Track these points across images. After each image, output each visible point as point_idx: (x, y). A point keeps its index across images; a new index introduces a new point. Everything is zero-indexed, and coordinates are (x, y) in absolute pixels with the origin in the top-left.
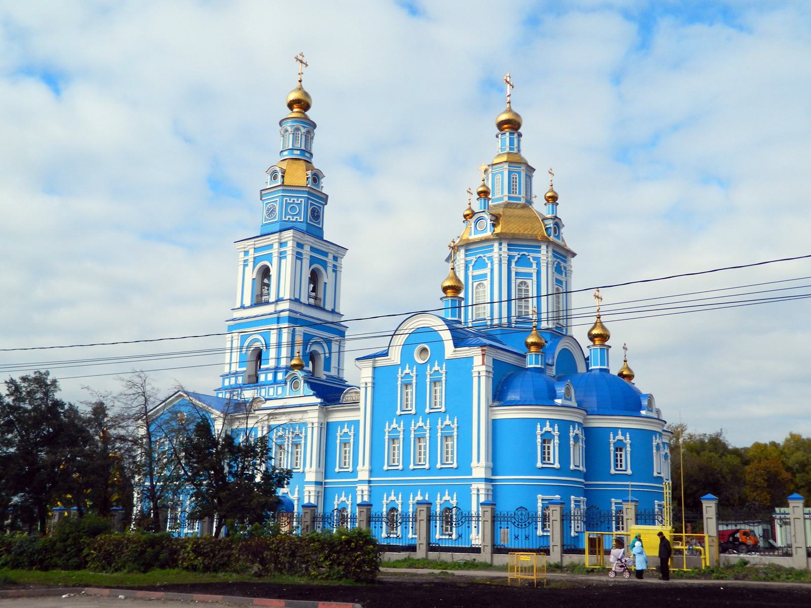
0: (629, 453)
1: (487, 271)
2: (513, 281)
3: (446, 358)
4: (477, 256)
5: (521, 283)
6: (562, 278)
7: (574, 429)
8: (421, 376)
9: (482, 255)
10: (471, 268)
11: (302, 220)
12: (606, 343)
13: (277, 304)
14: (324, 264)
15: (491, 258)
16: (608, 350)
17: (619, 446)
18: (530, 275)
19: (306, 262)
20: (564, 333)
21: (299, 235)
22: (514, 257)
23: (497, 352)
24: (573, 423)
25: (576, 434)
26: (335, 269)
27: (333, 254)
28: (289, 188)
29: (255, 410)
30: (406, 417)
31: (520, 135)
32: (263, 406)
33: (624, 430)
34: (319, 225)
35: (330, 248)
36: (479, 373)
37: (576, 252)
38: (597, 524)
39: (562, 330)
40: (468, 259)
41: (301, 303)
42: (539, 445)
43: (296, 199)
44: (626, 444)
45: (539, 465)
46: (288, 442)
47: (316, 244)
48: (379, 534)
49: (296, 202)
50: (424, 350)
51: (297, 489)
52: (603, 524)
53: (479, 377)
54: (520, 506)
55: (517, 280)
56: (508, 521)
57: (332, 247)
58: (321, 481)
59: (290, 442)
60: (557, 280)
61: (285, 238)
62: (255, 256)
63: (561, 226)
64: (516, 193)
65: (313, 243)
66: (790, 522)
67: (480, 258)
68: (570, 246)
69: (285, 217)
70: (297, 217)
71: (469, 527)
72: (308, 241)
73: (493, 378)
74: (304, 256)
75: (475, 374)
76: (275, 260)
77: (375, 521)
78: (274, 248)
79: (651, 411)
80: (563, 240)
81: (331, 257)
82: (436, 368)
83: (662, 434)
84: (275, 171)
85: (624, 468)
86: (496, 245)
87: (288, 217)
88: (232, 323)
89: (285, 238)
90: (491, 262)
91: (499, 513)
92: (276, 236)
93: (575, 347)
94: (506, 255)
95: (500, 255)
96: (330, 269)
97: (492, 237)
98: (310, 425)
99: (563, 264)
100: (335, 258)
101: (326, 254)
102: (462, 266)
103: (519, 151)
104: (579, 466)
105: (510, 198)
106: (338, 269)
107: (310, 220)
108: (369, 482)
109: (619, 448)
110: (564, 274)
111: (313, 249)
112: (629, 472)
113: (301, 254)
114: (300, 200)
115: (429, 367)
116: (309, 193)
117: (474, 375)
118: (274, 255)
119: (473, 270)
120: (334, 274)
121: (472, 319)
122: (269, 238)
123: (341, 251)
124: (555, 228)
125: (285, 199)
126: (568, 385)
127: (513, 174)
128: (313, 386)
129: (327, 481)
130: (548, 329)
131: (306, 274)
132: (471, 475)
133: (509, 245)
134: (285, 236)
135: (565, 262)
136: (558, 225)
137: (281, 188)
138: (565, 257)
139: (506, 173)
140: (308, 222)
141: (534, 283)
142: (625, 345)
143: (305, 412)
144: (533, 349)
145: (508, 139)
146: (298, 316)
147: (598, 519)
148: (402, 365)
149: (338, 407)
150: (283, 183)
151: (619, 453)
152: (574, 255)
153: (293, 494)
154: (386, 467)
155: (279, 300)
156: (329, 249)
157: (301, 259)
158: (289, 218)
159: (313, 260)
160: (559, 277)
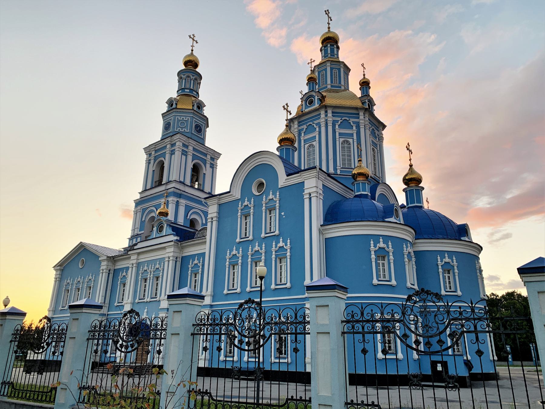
3: (279, 187)
4: (308, 125)
8: (258, 206)
9: (311, 123)
10: (303, 134)
11: (188, 131)
18: (352, 135)
19: (190, 158)
21: (185, 138)
22: (338, 121)
26: (213, 167)
27: (210, 155)
30: (245, 243)
31: (338, 48)
36: (310, 195)
42: (373, 260)
43: (184, 118)
44: (453, 266)
49: (184, 119)
50: (261, 185)
53: (310, 199)
54: (366, 314)
56: (363, 334)
59: (152, 275)
62: (156, 155)
67: (310, 126)
70: (185, 129)
76: (167, 156)
81: (209, 157)
86: (323, 112)
87: (178, 129)
90: (319, 127)
92: (169, 139)
95: (326, 120)
96: (208, 166)
98: (167, 259)
103: (338, 57)
104: (414, 285)
105: (332, 86)
106: (215, 166)
108: (211, 306)
117: (305, 197)
122: (164, 142)
127: (334, 70)
131: (190, 166)
133: (333, 112)
137: (175, 110)
139: (329, 69)
143: (164, 248)
145: (329, 49)
148: (242, 199)
154: (225, 292)
155: (169, 182)
156: (207, 151)
157: (186, 156)
159: (194, 157)
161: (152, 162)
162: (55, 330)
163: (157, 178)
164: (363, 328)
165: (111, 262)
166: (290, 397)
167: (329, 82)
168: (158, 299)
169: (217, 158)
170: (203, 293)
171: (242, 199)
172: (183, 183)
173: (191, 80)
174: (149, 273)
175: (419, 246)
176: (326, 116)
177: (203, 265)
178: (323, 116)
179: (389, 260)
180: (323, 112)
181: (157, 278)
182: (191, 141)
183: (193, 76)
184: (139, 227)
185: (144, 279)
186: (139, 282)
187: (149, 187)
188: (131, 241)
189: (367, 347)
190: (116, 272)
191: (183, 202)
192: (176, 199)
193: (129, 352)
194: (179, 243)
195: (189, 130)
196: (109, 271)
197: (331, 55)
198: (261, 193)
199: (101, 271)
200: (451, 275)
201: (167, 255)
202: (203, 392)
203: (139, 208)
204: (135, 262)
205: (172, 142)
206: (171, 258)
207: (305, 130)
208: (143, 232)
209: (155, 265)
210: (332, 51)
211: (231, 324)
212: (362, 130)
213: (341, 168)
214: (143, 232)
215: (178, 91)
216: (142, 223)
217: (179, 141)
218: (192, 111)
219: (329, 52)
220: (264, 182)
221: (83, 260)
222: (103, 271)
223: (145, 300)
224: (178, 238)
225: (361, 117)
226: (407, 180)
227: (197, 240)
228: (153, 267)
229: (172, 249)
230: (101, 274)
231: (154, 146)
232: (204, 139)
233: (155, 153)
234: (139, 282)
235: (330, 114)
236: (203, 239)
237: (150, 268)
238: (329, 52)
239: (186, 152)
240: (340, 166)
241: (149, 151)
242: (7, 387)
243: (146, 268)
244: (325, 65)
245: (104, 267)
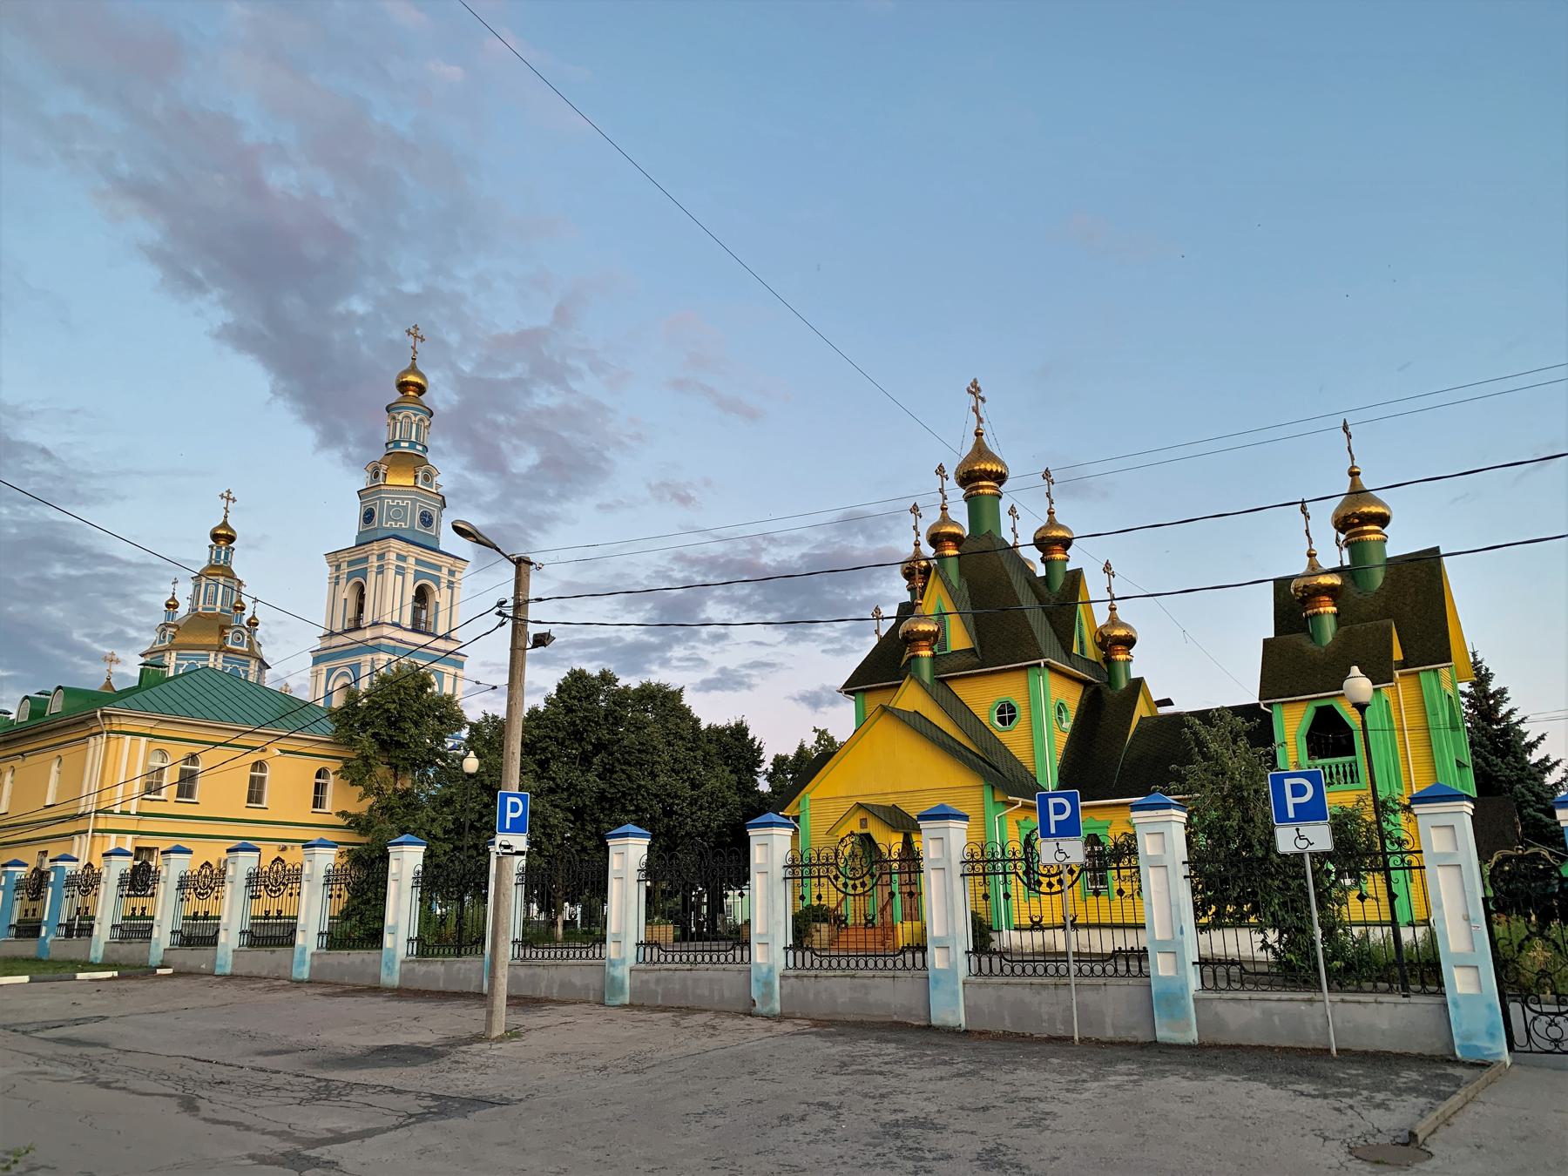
14: (437, 580)
19: (410, 578)
26: (451, 585)
41: (401, 627)
56: (1005, 874)
57: (445, 558)
76: (371, 577)
77: (984, 874)
96: (444, 585)
100: (451, 573)
101: (439, 568)
111: (418, 562)
123: (459, 564)
131: (411, 592)
157: (403, 575)
159: (417, 575)
161: (343, 582)
162: (289, 871)
163: (351, 613)
164: (984, 869)
166: (1117, 949)
183: (415, 415)
193: (859, 895)
202: (913, 947)
203: (323, 667)
211: (832, 864)
218: (415, 489)
239: (403, 568)
242: (648, 950)
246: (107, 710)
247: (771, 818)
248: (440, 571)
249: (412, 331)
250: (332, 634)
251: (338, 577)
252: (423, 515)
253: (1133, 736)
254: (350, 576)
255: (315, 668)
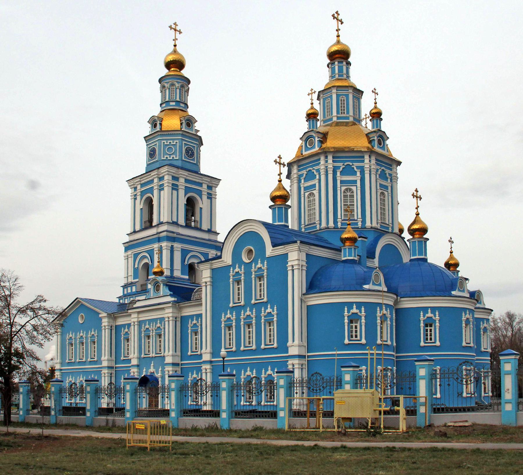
0: (363, 324)
1: (316, 182)
2: (339, 189)
3: (267, 256)
4: (307, 170)
5: (347, 189)
6: (388, 183)
7: (466, 314)
8: (248, 274)
9: (311, 169)
10: (303, 181)
11: (177, 158)
12: (425, 236)
13: (158, 227)
14: (200, 193)
15: (318, 171)
16: (425, 242)
17: (429, 322)
18: (355, 182)
19: (182, 192)
20: (390, 231)
21: (173, 170)
22: (339, 167)
23: (310, 248)
24: (380, 305)
25: (467, 319)
26: (211, 197)
28: (166, 133)
29: (128, 310)
30: (238, 309)
31: (349, 64)
32: (135, 306)
33: (433, 309)
34: (194, 161)
35: (203, 179)
37: (401, 161)
38: (320, 389)
39: (388, 228)
40: (300, 173)
42: (346, 324)
43: (172, 141)
44: (435, 320)
45: (346, 341)
46: (153, 333)
47: (189, 177)
48: (187, 402)
49: (172, 143)
50: (250, 251)
51: (160, 369)
52: (326, 389)
53: (293, 270)
55: (342, 187)
58: (178, 362)
59: (154, 333)
60: (381, 185)
61: (162, 173)
63: (385, 138)
64: (344, 113)
65: (187, 176)
66: (356, 388)
68: (396, 155)
69: (163, 157)
71: (217, 396)
72: (182, 174)
73: (306, 271)
74: (180, 187)
75: (290, 268)
76: (156, 192)
78: (155, 182)
79: (463, 291)
80: (388, 150)
82: (259, 265)
83: (474, 311)
84: (155, 121)
85: (433, 341)
86: (322, 158)
87: (166, 156)
88: (127, 245)
89: (162, 173)
91: (118, 387)
92: (155, 172)
93: (400, 243)
94: (332, 166)
95: (326, 167)
96: (205, 197)
97: (320, 151)
98: (167, 319)
99: (388, 172)
102: (295, 180)
103: (348, 77)
105: (338, 118)
106: (213, 196)
107: (185, 157)
108: (211, 362)
109: (429, 323)
110: (389, 180)
111: (187, 181)
112: (438, 343)
113: (177, 186)
114: (175, 141)
115: (253, 265)
116: (182, 135)
118: (155, 188)
119: (304, 182)
120: (209, 200)
121: (305, 224)
124: (379, 140)
125: (163, 142)
126: (376, 272)
128: (171, 288)
129: (182, 362)
130: (372, 228)
131: (183, 201)
132: (287, 353)
133: (333, 157)
134: (162, 172)
135: (391, 170)
136: (382, 137)
137: (159, 133)
138: (391, 166)
139: (334, 97)
140: (183, 159)
141: (358, 188)
142: (451, 238)
143: (163, 309)
144: (347, 244)
145: (337, 68)
146: (175, 235)
147: (321, 384)
148: (233, 265)
149: (187, 304)
150: (161, 129)
151: (429, 328)
152: (399, 163)
153: (158, 373)
155: (161, 223)
157: (177, 190)
158: (167, 157)
159: (187, 190)
160: (384, 183)
161: (139, 198)
163: (146, 218)
165: (112, 318)
167: (335, 113)
168: (162, 355)
169: (215, 185)
170: (167, 407)
171: (233, 265)
172: (175, 224)
173: (176, 89)
174: (151, 331)
175: (403, 304)
176: (327, 162)
177: (201, 325)
178: (322, 162)
179: (361, 323)
180: (322, 158)
181: (160, 336)
182: (181, 172)
184: (132, 275)
185: (147, 336)
186: (143, 339)
187: (138, 228)
188: (126, 290)
189: (450, 383)
190: (118, 328)
191: (177, 246)
192: (170, 244)
194: (177, 304)
195: (178, 157)
196: (111, 327)
197: (339, 76)
198: (252, 260)
199: (103, 328)
200: (433, 328)
201: (166, 315)
203: (130, 252)
204: (136, 320)
205: (159, 175)
206: (171, 319)
207: (304, 175)
208: (137, 280)
209: (156, 323)
210: (340, 70)
211: (455, 373)
212: (367, 176)
213: (342, 220)
214: (137, 280)
215: (161, 105)
216: (136, 270)
217: (168, 174)
218: (181, 133)
219: (337, 71)
220: (253, 250)
221: (82, 315)
222: (105, 327)
223: (150, 356)
224: (176, 299)
225: (367, 160)
226: (412, 230)
227: (194, 302)
228: (154, 326)
229: (170, 310)
230: (103, 331)
231: (139, 180)
232: (197, 165)
233: (141, 187)
234: (143, 339)
235: (330, 160)
236: (199, 301)
237: (151, 326)
238: (337, 71)
240: (341, 219)
241: (134, 185)
243: (147, 326)
244: (330, 92)
245: (106, 324)
246: (59, 336)
247: (351, 364)
248: (202, 186)
249: (173, 26)
250: (135, 232)
251: (135, 195)
252: (187, 151)
253: (356, 363)
254: (143, 193)
255: (126, 254)
